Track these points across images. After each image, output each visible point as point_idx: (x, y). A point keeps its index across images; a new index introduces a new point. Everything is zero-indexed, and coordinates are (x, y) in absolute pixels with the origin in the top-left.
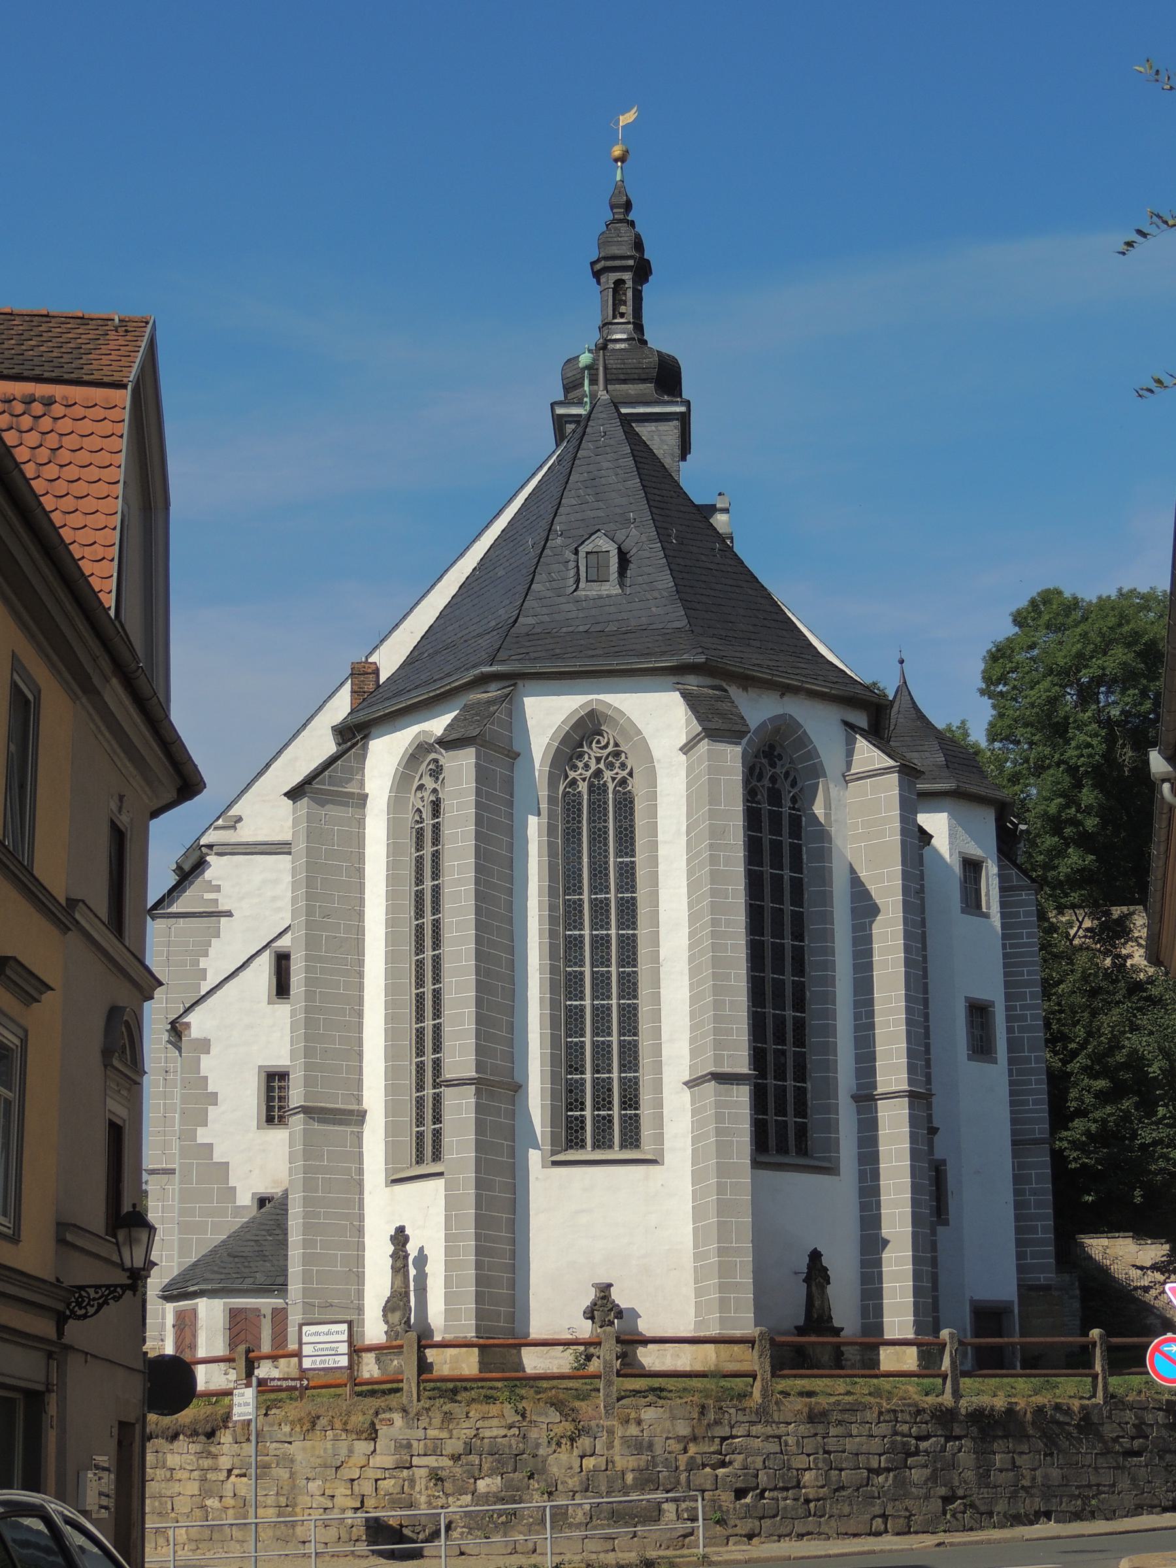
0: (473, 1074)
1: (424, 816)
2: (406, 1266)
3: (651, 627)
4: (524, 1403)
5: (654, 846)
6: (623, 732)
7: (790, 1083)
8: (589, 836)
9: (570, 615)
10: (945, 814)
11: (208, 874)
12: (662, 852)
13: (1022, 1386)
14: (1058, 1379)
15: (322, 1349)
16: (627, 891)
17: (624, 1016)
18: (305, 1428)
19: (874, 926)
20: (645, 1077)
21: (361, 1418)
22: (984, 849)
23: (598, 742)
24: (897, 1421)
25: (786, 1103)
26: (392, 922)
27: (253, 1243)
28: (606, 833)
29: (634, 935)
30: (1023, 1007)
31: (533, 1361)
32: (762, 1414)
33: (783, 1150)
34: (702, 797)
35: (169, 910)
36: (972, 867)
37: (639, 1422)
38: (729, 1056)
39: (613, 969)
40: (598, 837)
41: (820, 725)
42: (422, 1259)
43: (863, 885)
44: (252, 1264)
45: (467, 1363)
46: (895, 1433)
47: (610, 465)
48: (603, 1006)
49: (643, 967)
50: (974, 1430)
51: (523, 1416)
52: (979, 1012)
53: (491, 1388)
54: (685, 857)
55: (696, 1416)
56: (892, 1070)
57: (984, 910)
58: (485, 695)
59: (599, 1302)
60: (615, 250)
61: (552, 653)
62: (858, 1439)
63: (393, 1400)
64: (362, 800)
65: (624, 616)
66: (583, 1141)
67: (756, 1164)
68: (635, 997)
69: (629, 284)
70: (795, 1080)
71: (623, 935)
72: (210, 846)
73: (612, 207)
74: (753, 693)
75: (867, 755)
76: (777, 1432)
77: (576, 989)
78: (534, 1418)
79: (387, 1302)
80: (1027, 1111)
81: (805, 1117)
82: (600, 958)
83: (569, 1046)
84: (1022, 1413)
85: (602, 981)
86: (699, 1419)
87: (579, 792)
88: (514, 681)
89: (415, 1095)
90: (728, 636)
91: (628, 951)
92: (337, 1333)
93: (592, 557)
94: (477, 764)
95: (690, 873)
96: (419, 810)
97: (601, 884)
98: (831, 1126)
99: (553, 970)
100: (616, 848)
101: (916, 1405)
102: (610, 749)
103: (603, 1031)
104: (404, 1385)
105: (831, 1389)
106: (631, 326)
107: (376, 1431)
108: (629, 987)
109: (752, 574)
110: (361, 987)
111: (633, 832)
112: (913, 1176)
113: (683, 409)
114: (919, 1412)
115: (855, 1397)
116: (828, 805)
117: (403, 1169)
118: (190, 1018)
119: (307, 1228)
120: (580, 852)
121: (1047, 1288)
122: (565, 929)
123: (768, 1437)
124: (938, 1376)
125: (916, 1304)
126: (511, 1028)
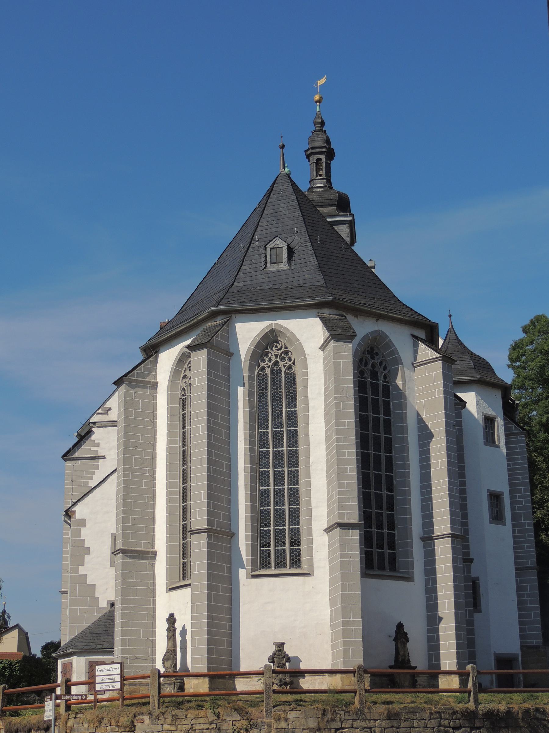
0: (206, 527)
1: (186, 392)
2: (174, 635)
3: (305, 285)
4: (219, 710)
5: (306, 401)
6: (289, 340)
7: (385, 531)
8: (272, 397)
9: (261, 281)
10: (474, 393)
11: (93, 437)
12: (311, 404)
13: (517, 698)
14: (539, 694)
15: (106, 679)
16: (293, 426)
17: (291, 494)
18: (95, 725)
19: (431, 444)
20: (303, 527)
21: (126, 719)
22: (495, 410)
23: (276, 346)
24: (441, 719)
25: (382, 540)
26: (170, 449)
27: (103, 626)
28: (281, 395)
29: (297, 450)
30: (520, 497)
31: (242, 685)
32: (360, 714)
33: (382, 567)
34: (332, 371)
35: (73, 456)
36: (489, 421)
37: (286, 720)
38: (347, 514)
39: (285, 469)
40: (277, 397)
41: (399, 337)
42: (184, 632)
43: (424, 422)
44: (101, 638)
45: (201, 686)
46: (440, 725)
47: (285, 205)
48: (280, 489)
49: (302, 467)
50: (488, 723)
51: (218, 717)
52: (495, 498)
53: (203, 701)
54: (324, 406)
55: (320, 716)
56: (442, 524)
57: (497, 444)
58: (215, 323)
59: (277, 653)
60: (317, 144)
61: (250, 299)
62: (418, 729)
63: (145, 709)
64: (155, 385)
65: (291, 280)
66: (270, 564)
67: (365, 575)
68: (298, 484)
69: (324, 160)
70: (388, 530)
71: (290, 450)
72: (94, 423)
73: (315, 124)
74: (360, 319)
75: (425, 352)
76: (369, 725)
77: (265, 481)
78: (225, 718)
79: (165, 655)
80: (526, 552)
81: (394, 549)
82: (278, 463)
83: (261, 512)
84: (516, 714)
85: (279, 476)
86: (322, 718)
87: (266, 374)
88: (230, 314)
89: (182, 542)
90: (349, 293)
91: (293, 459)
92: (115, 669)
93: (274, 251)
94: (208, 357)
95: (326, 414)
96: (184, 389)
97: (278, 423)
98: (409, 554)
99: (252, 470)
100: (286, 403)
101: (452, 709)
102: (283, 350)
103: (280, 503)
104: (151, 700)
105: (402, 700)
106: (325, 180)
107: (135, 726)
108: (294, 479)
109: (362, 260)
110: (154, 485)
111: (295, 394)
112: (455, 581)
113: (350, 218)
114: (455, 713)
115: (416, 704)
116: (404, 379)
117: (176, 583)
118: (76, 509)
119: (123, 616)
120: (267, 406)
121: (537, 647)
122: (259, 448)
123: (364, 728)
124: (466, 692)
125: (458, 653)
126: (229, 502)
